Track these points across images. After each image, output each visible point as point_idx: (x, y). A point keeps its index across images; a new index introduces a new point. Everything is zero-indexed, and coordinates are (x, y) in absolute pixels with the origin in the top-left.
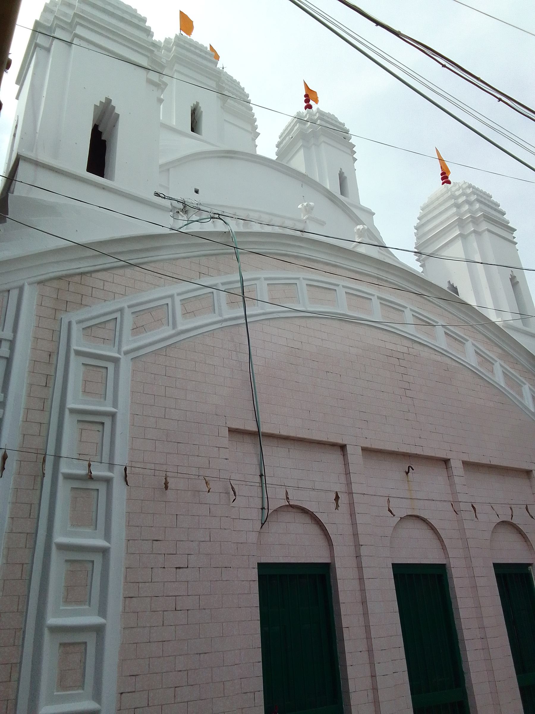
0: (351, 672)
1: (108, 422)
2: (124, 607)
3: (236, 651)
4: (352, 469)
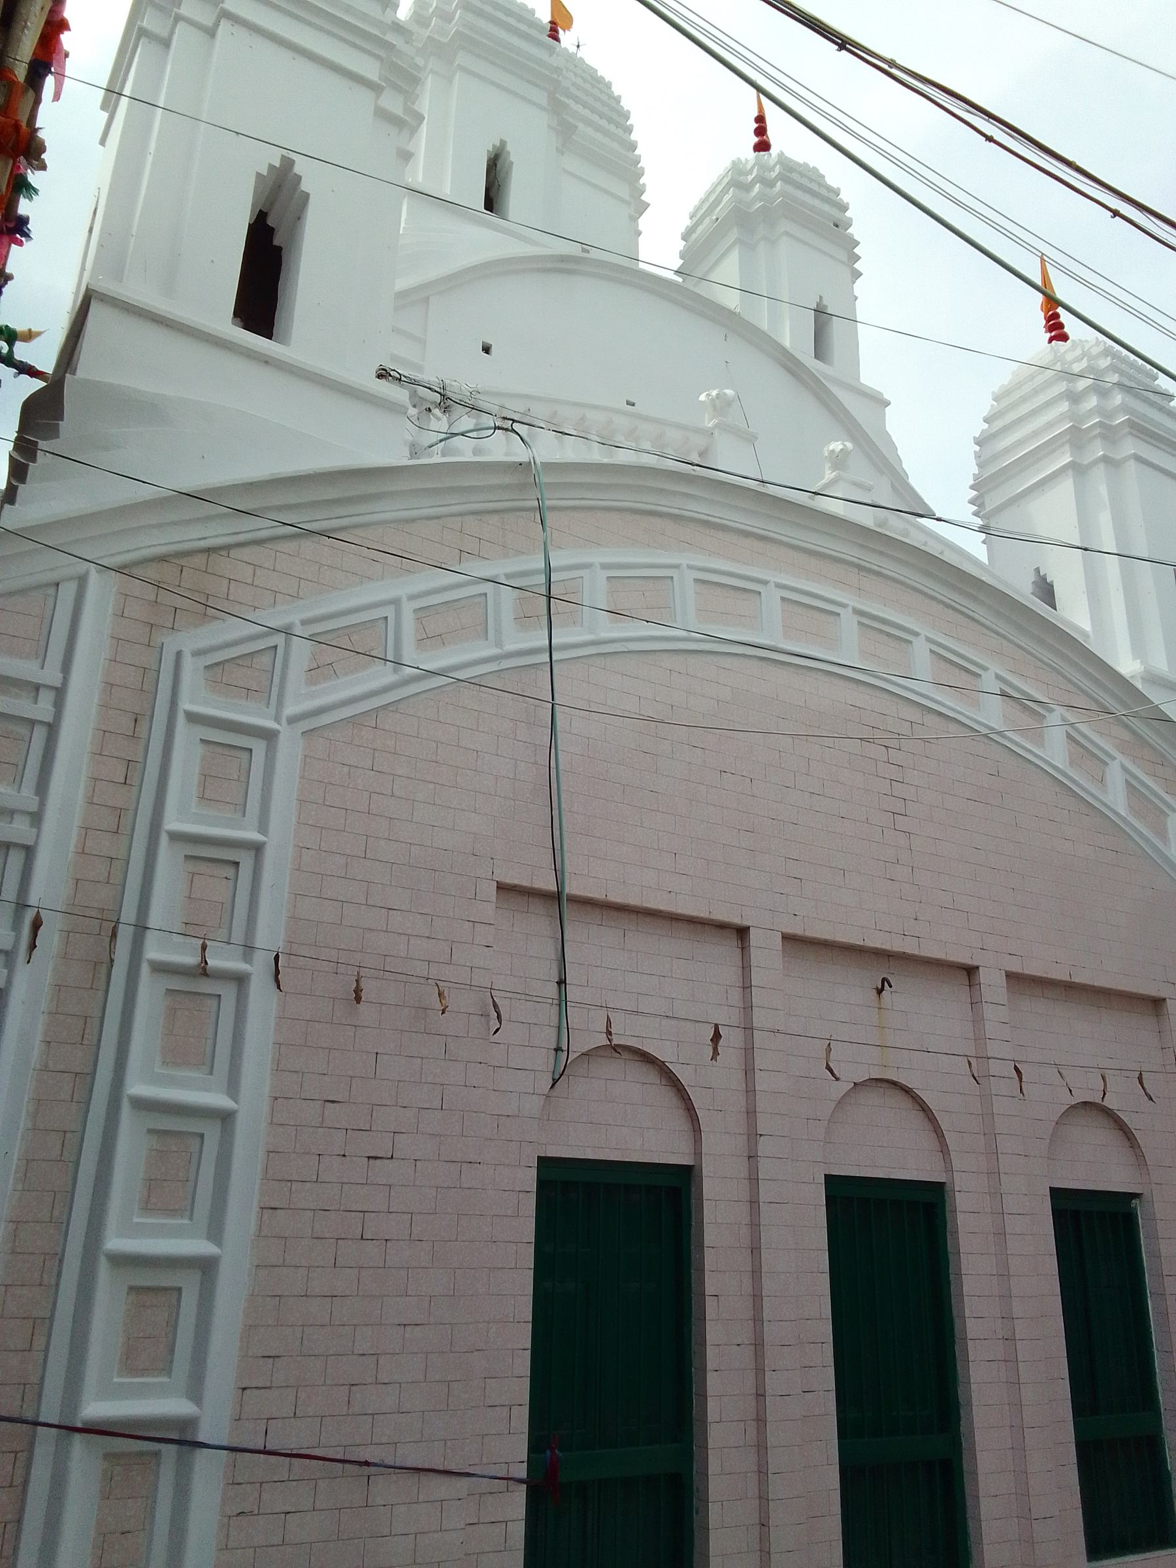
0: (714, 1384)
1: (246, 860)
3: (480, 1326)
4: (757, 978)
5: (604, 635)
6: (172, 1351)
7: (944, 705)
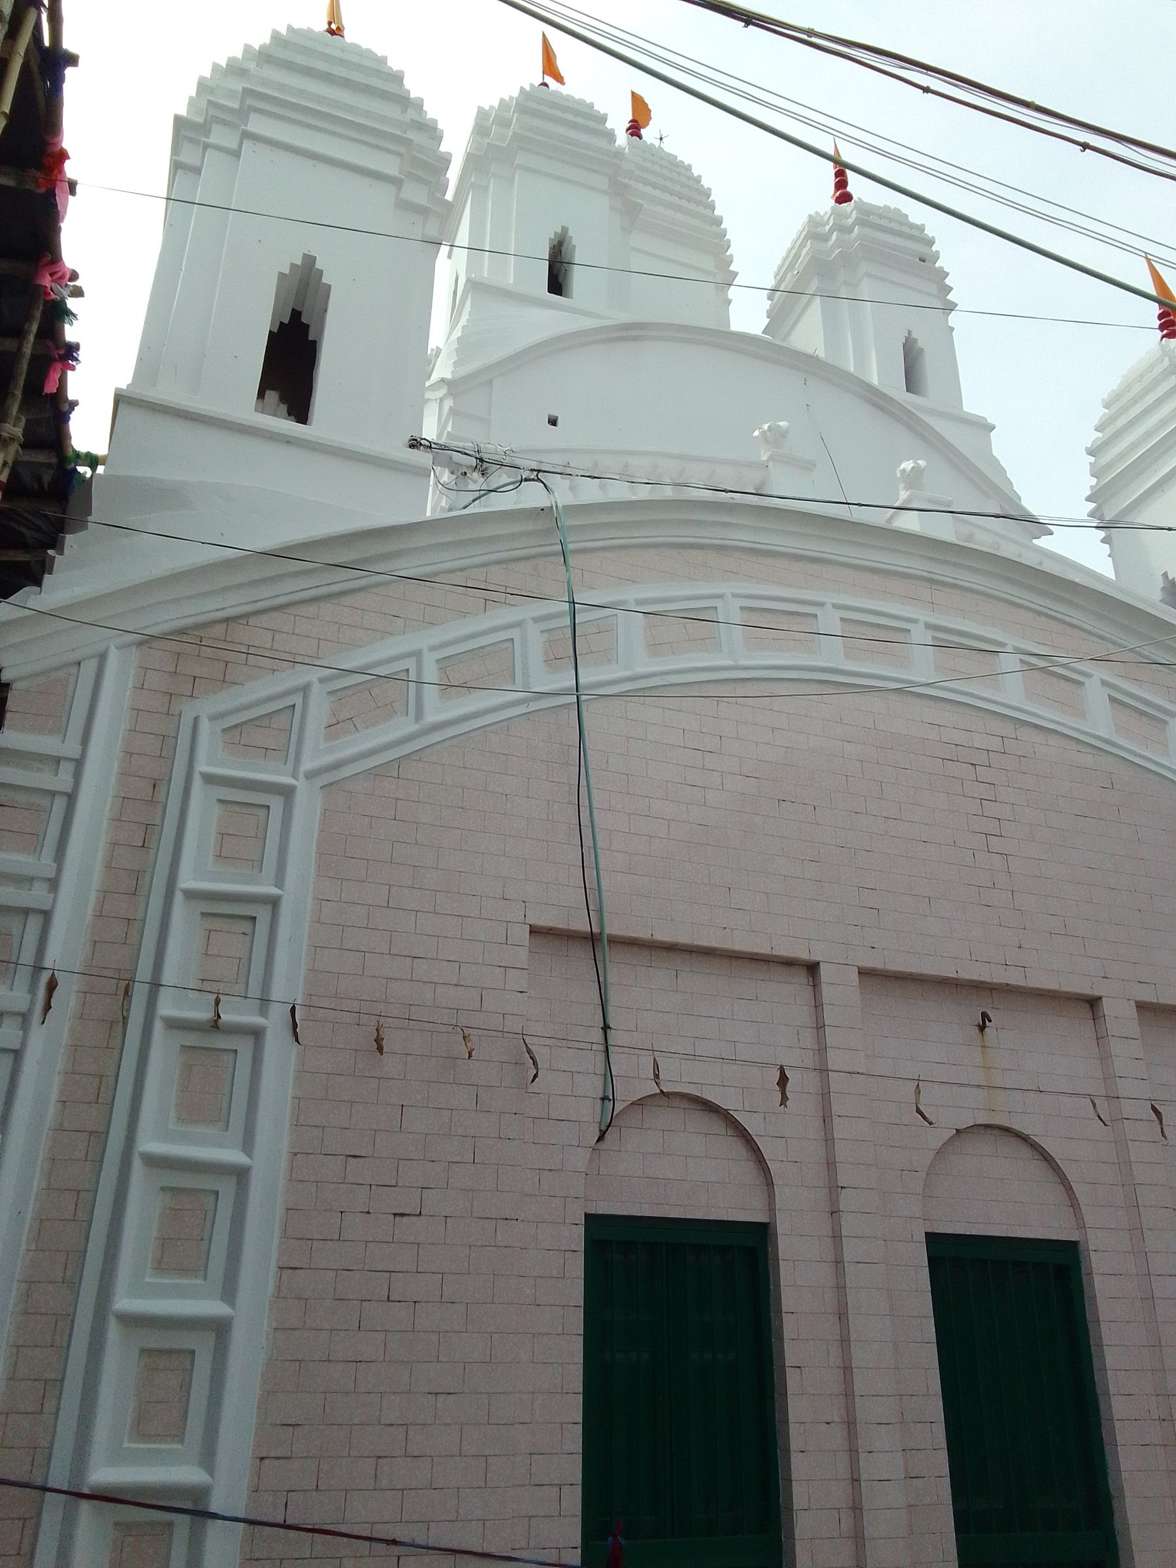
2: (279, 1287)
4: (829, 1016)
5: (641, 670)
6: (185, 1416)
7: (1044, 718)
